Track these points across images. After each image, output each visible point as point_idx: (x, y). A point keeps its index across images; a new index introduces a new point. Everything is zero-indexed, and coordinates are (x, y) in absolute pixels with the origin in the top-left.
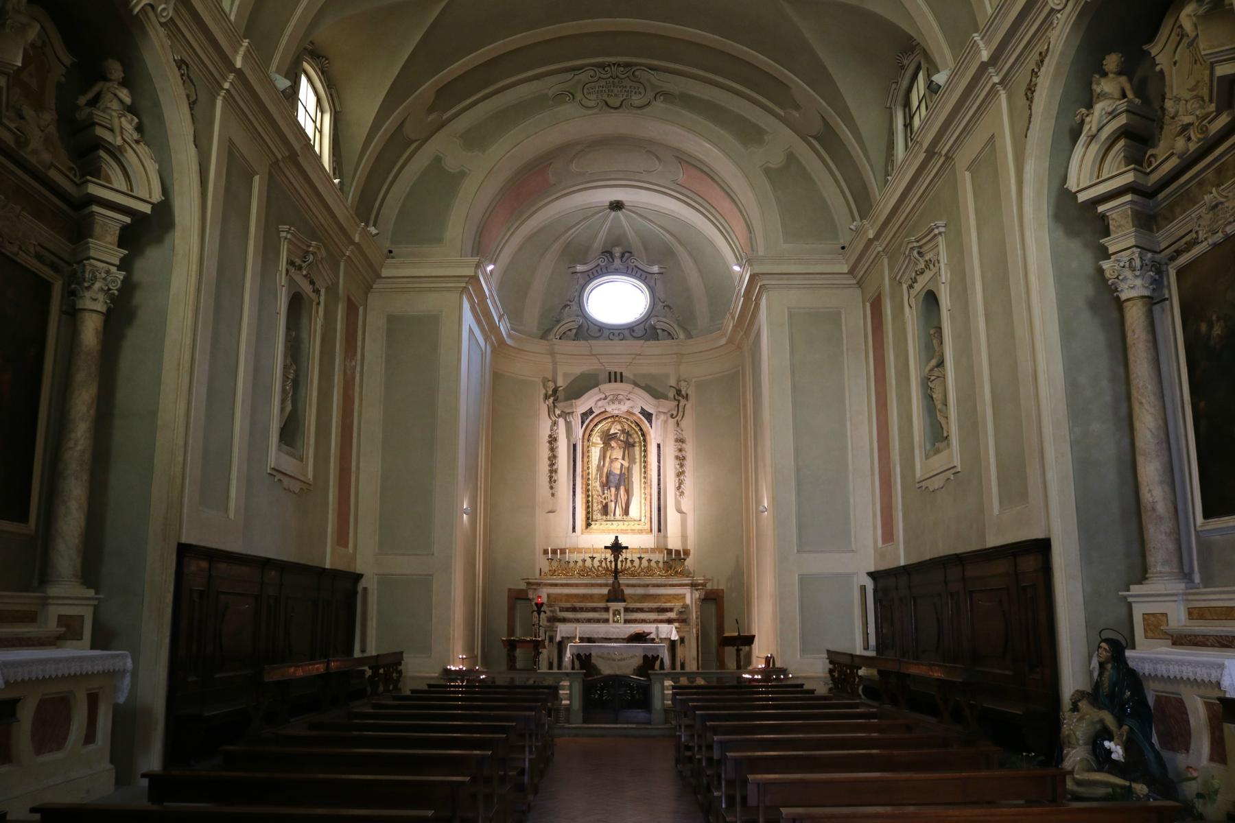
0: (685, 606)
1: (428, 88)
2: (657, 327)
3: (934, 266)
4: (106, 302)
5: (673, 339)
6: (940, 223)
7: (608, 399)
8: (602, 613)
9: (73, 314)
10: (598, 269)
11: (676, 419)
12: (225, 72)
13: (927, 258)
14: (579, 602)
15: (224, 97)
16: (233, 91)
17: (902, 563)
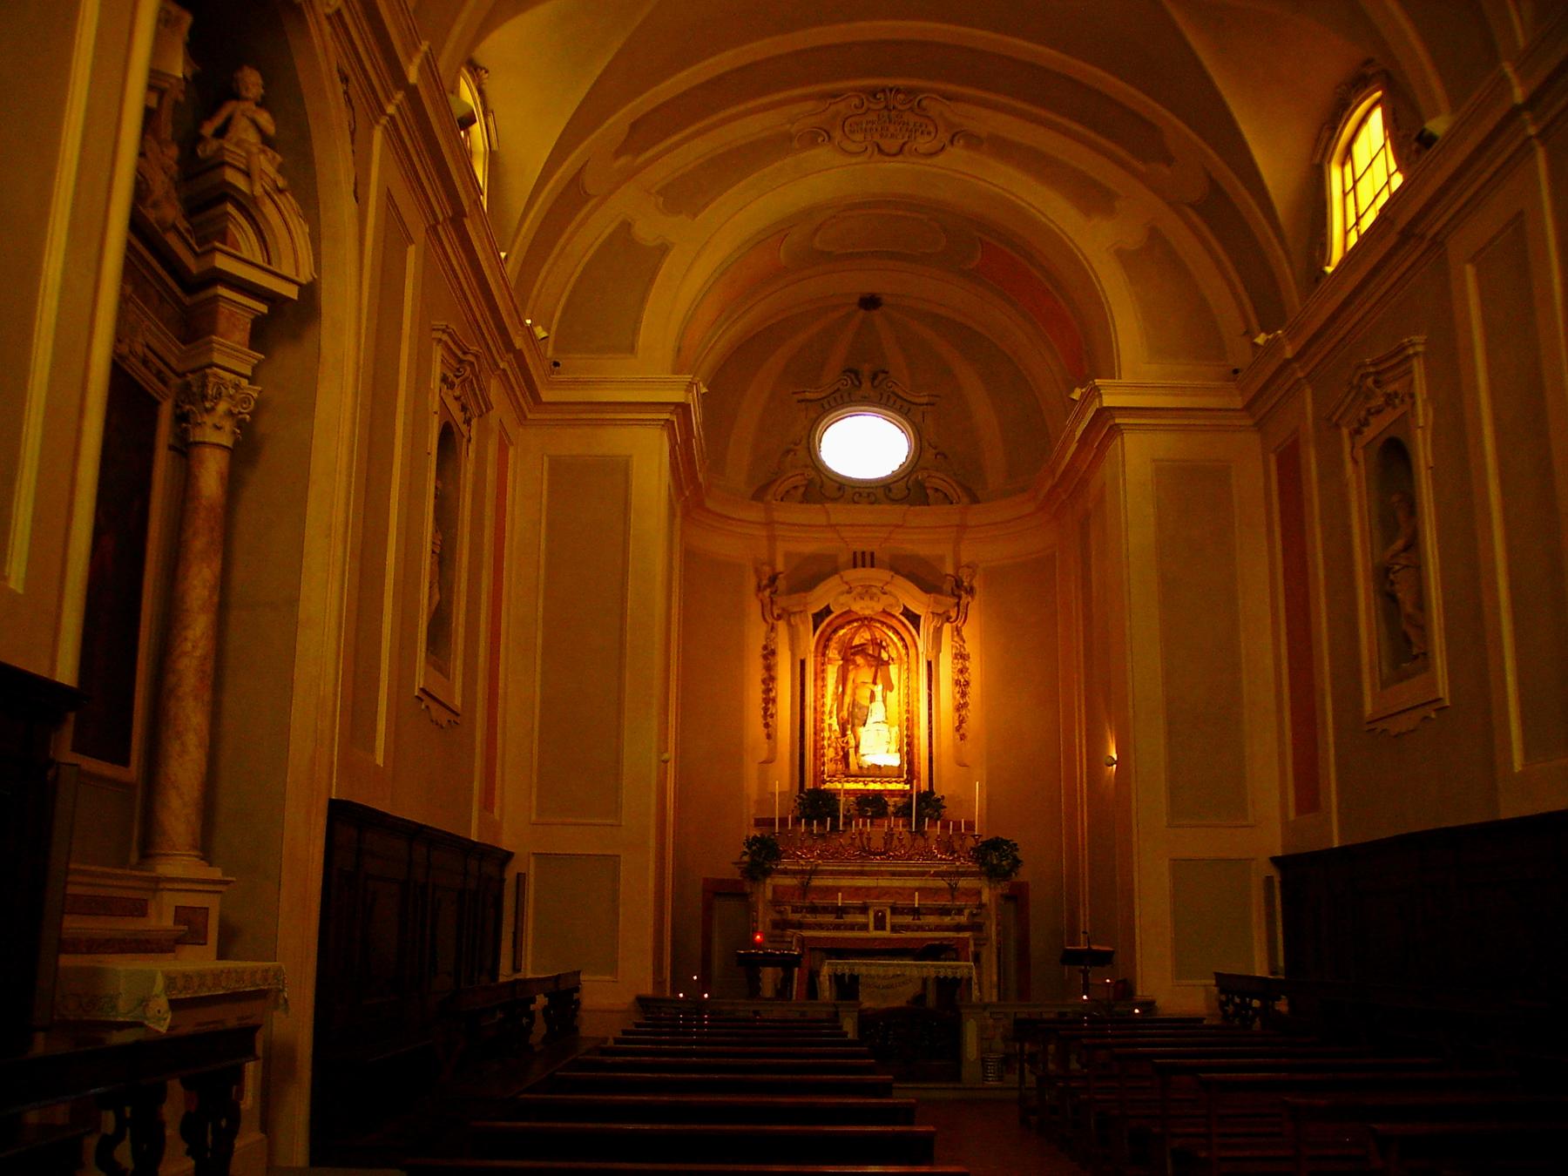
0: (981, 906)
1: (618, 122)
2: (927, 484)
3: (1403, 400)
4: (234, 433)
5: (952, 503)
6: (1416, 338)
7: (854, 593)
8: (857, 915)
9: (185, 449)
10: (837, 395)
11: (954, 624)
12: (392, 88)
13: (1391, 389)
14: (821, 899)
15: (385, 127)
16: (398, 118)
17: (1336, 844)
